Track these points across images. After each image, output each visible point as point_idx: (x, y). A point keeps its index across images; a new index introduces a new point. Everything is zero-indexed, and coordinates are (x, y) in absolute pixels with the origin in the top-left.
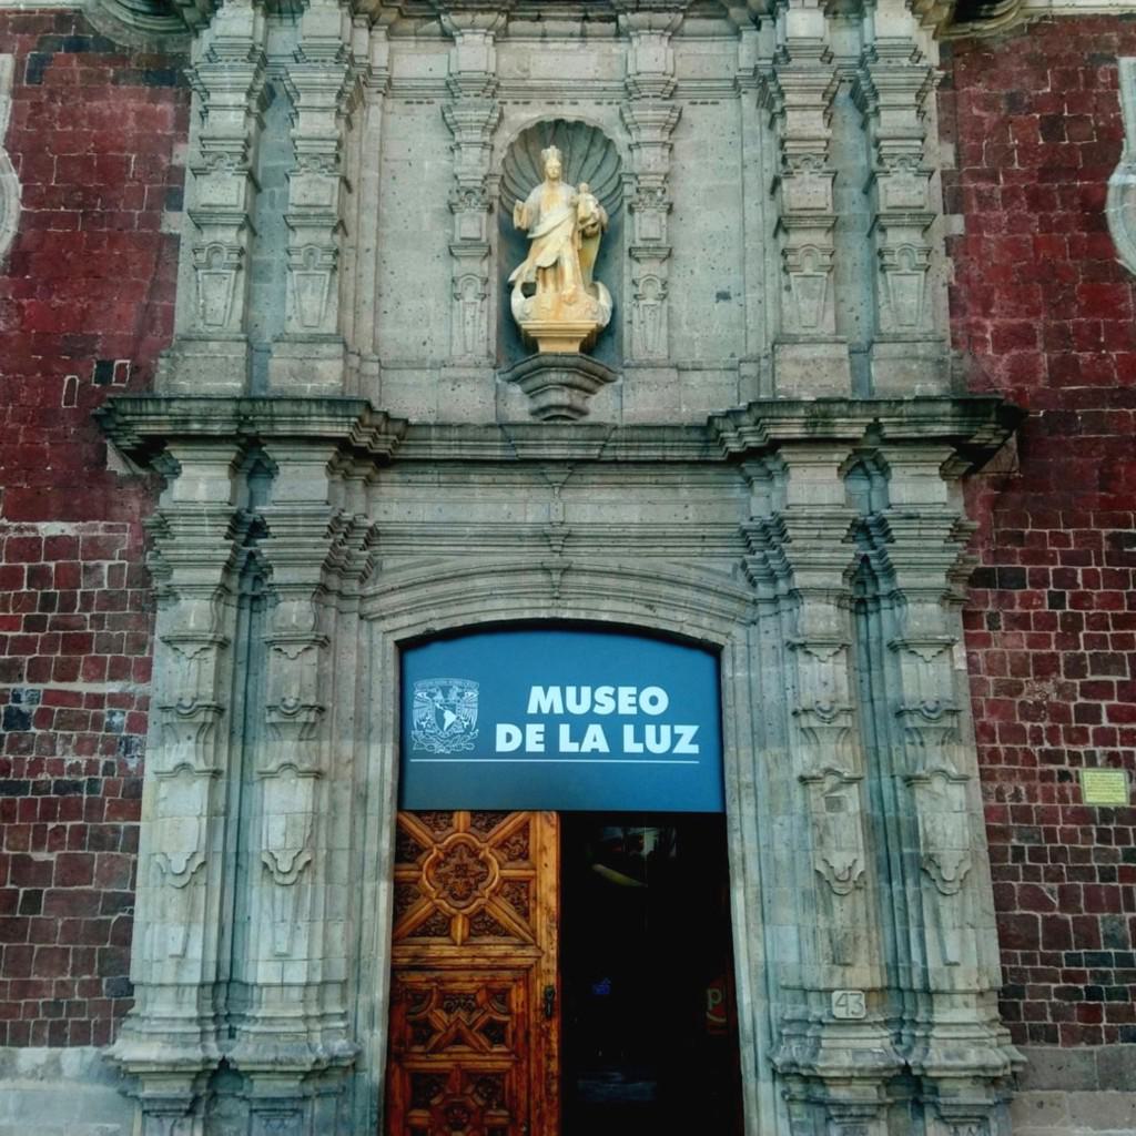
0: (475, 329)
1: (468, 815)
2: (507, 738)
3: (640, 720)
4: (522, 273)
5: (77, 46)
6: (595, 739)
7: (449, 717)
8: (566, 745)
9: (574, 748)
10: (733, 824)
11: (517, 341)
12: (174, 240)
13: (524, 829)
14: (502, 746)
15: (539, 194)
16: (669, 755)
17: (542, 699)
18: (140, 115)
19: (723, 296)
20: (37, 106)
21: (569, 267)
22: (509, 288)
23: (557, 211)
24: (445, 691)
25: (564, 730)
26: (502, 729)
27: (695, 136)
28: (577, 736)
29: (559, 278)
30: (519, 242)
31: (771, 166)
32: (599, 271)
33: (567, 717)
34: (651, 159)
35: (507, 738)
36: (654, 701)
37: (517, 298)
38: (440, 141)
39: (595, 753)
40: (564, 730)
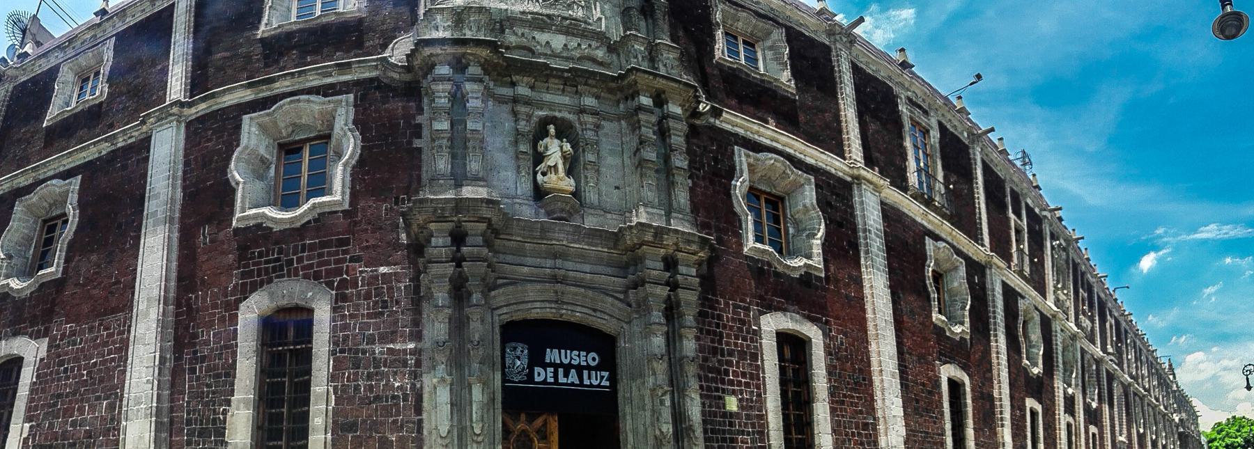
0: (525, 187)
1: (572, 189)
2: (540, 374)
3: (589, 368)
4: (542, 167)
5: (378, 88)
6: (573, 377)
7: (519, 363)
8: (562, 380)
9: (565, 380)
10: (625, 410)
11: (539, 193)
12: (419, 150)
13: (545, 424)
14: (537, 379)
15: (547, 140)
16: (599, 386)
17: (552, 355)
18: (403, 108)
19: (617, 188)
20: (365, 109)
21: (560, 167)
22: (535, 173)
23: (555, 150)
24: (515, 348)
25: (561, 371)
26: (537, 369)
27: (605, 131)
28: (566, 375)
29: (556, 172)
30: (539, 158)
31: (635, 144)
32: (569, 173)
33: (561, 365)
34: (590, 134)
35: (540, 374)
36: (594, 359)
37: (539, 177)
38: (511, 118)
39: (573, 384)
40: (561, 371)
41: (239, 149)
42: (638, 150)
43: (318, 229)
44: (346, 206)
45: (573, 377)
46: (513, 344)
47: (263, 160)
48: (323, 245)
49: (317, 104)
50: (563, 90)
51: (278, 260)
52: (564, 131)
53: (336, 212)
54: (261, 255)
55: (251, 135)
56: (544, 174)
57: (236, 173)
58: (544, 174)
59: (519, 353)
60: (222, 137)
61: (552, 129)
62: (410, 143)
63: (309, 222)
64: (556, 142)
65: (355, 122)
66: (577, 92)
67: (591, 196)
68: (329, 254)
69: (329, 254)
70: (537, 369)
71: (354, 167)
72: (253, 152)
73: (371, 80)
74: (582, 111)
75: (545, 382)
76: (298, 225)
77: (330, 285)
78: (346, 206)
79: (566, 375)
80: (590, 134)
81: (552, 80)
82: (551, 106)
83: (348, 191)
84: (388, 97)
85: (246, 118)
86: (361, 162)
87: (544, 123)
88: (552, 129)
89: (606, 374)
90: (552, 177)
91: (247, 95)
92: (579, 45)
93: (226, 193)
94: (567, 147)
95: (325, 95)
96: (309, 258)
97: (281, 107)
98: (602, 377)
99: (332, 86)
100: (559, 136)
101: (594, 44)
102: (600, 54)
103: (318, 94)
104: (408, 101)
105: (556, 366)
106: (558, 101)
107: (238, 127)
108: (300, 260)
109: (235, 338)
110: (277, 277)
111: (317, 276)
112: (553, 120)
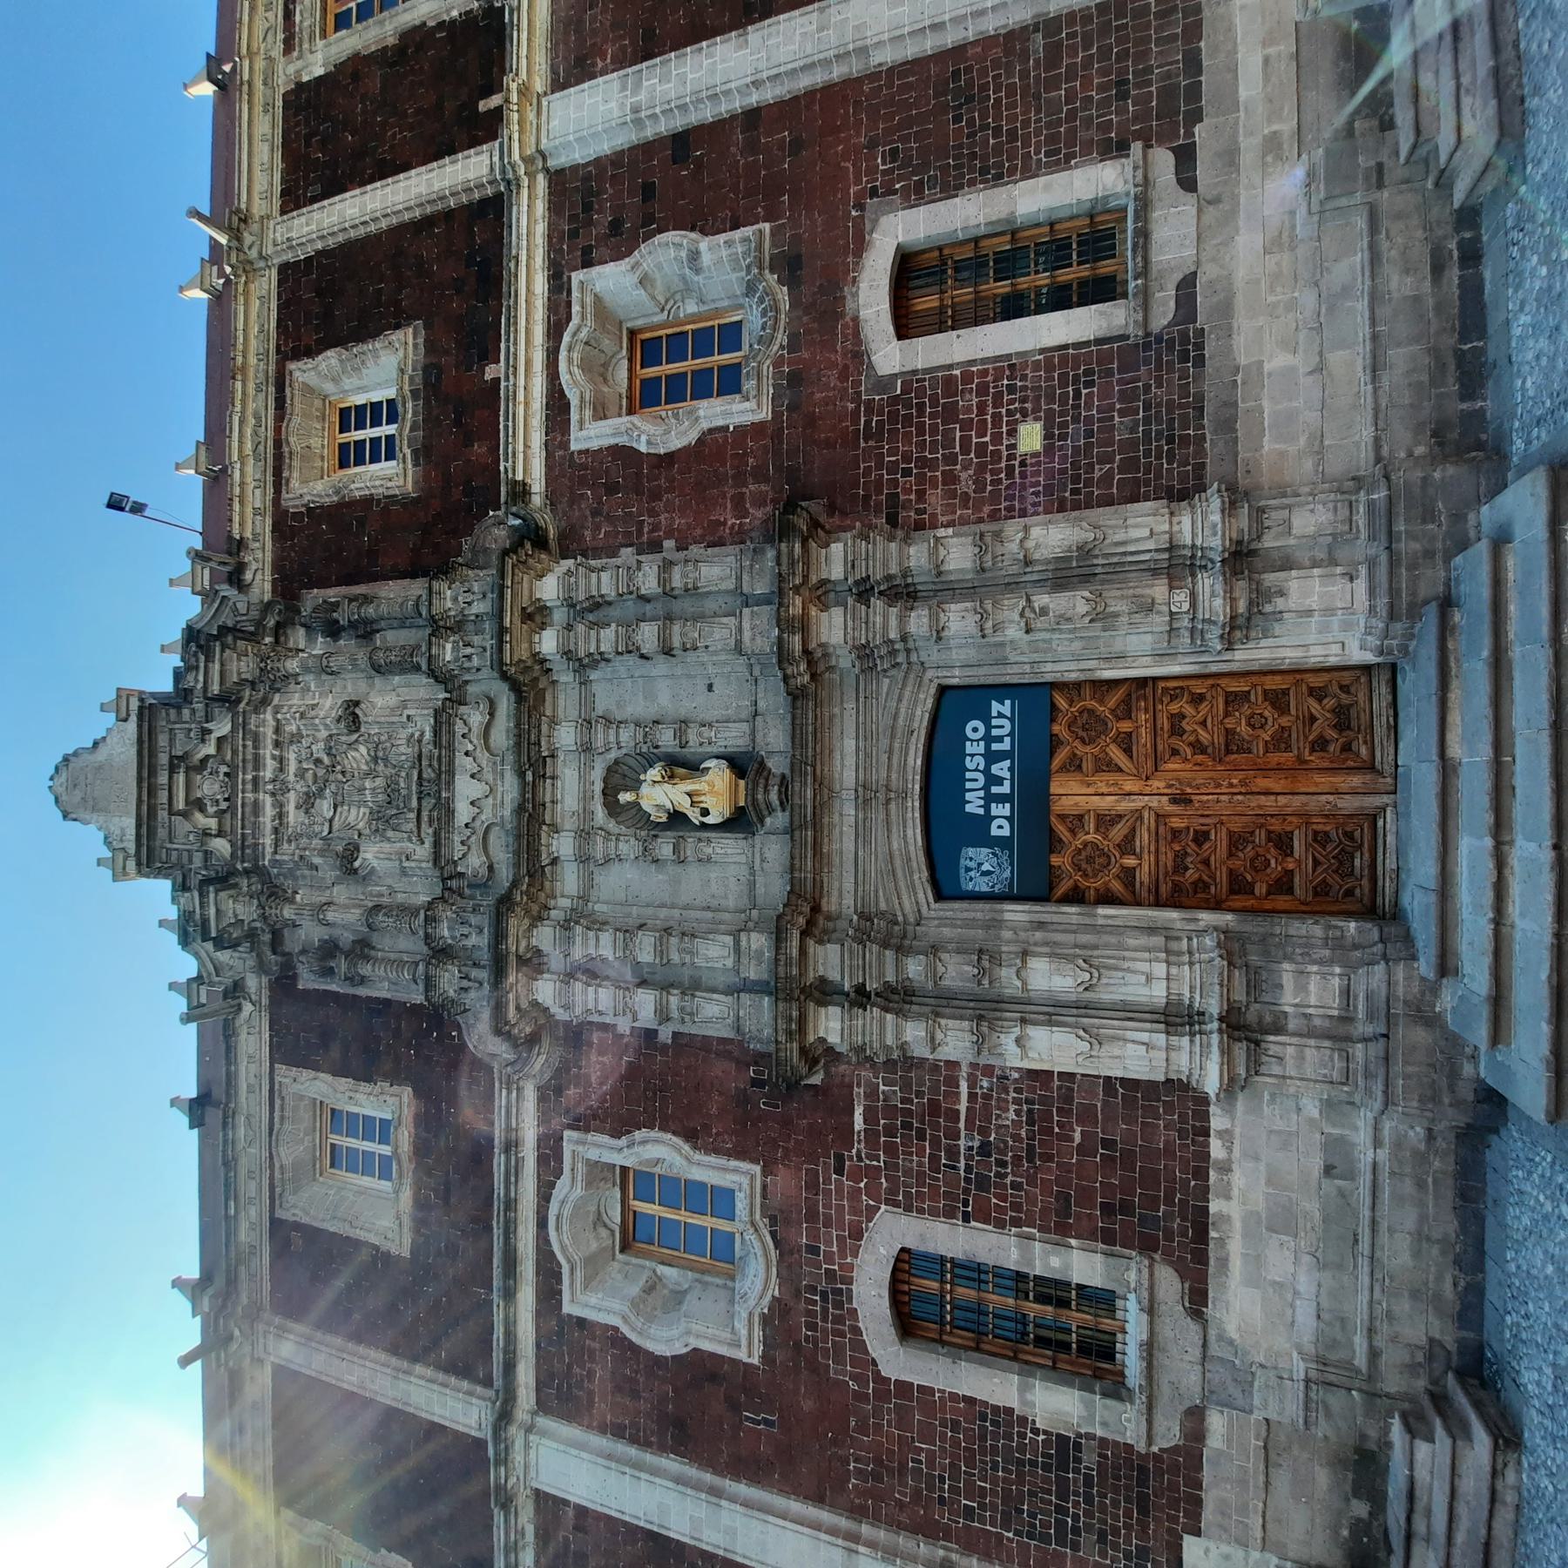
0: (729, 848)
4: (694, 816)
6: (1001, 769)
9: (1007, 783)
11: (740, 822)
14: (1006, 832)
16: (1012, 720)
17: (974, 806)
18: (600, 1053)
19: (710, 688)
22: (704, 826)
24: (968, 869)
25: (995, 790)
26: (995, 832)
28: (999, 781)
30: (677, 819)
31: (631, 660)
33: (986, 788)
35: (1000, 829)
36: (975, 730)
37: (709, 820)
38: (615, 868)
39: (1011, 769)
40: (995, 790)
41: (625, 1330)
42: (643, 656)
43: (787, 1222)
44: (757, 1169)
45: (1001, 769)
46: (962, 871)
47: (650, 1289)
48: (812, 1216)
49: (566, 1189)
50: (553, 778)
51: (824, 1295)
52: (620, 778)
53: (764, 1187)
54: (812, 1326)
55: (596, 1302)
56: (705, 812)
57: (665, 1339)
58: (705, 812)
59: (972, 864)
60: (592, 1352)
61: (625, 797)
62: (664, 1048)
63: (773, 1234)
64: (645, 789)
65: (616, 1134)
66: (553, 756)
67: (734, 738)
68: (827, 1206)
69: (827, 1206)
70: (995, 832)
71: (695, 1148)
72: (635, 1304)
73: (542, 1099)
74: (586, 748)
75: (1010, 819)
76: (773, 1254)
77: (872, 1212)
78: (757, 1169)
79: (999, 781)
80: (626, 735)
81: (539, 798)
82: (586, 798)
83: (734, 1163)
84: (577, 1076)
85: (567, 1308)
86: (691, 1136)
87: (613, 807)
88: (625, 797)
89: (995, 707)
90: (708, 801)
91: (527, 1297)
92: (467, 754)
93: (700, 1369)
94: (654, 773)
95: (558, 1173)
96: (829, 1243)
97: (563, 1248)
98: (1000, 715)
99: (542, 1160)
100: (636, 786)
101: (459, 728)
102: (476, 718)
103: (552, 1185)
104: (590, 1044)
105: (990, 799)
106: (572, 788)
107: (581, 1323)
108: (829, 1258)
109: (931, 1391)
110: (850, 1299)
111: (857, 1234)
112: (610, 794)
